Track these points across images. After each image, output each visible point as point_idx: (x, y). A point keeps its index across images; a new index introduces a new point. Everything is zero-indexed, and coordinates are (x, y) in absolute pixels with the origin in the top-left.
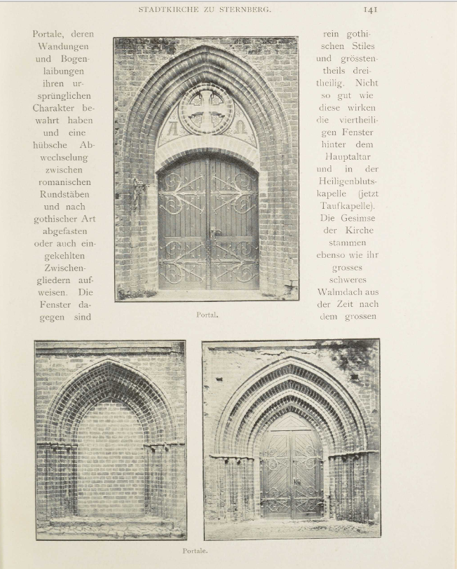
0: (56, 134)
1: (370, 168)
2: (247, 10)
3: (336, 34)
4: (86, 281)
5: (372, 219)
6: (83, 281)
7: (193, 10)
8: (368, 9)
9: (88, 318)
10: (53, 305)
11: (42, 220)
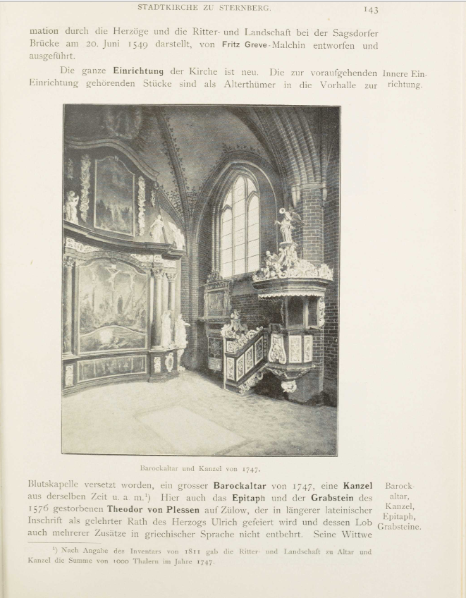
1: (52, 495)
2: (247, 9)
3: (365, 47)
7: (193, 8)
8: (368, 9)
10: (43, 44)
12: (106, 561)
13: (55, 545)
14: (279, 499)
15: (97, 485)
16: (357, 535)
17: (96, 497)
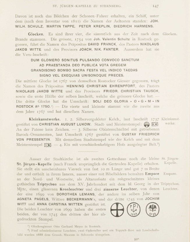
0: (61, 34)
4: (60, 135)
5: (158, 199)
6: (59, 135)
9: (30, 174)
11: (20, 184)
12: (61, 235)
13: (29, 224)
14: (28, 174)
15: (85, 145)
16: (58, 200)
17: (133, 34)
